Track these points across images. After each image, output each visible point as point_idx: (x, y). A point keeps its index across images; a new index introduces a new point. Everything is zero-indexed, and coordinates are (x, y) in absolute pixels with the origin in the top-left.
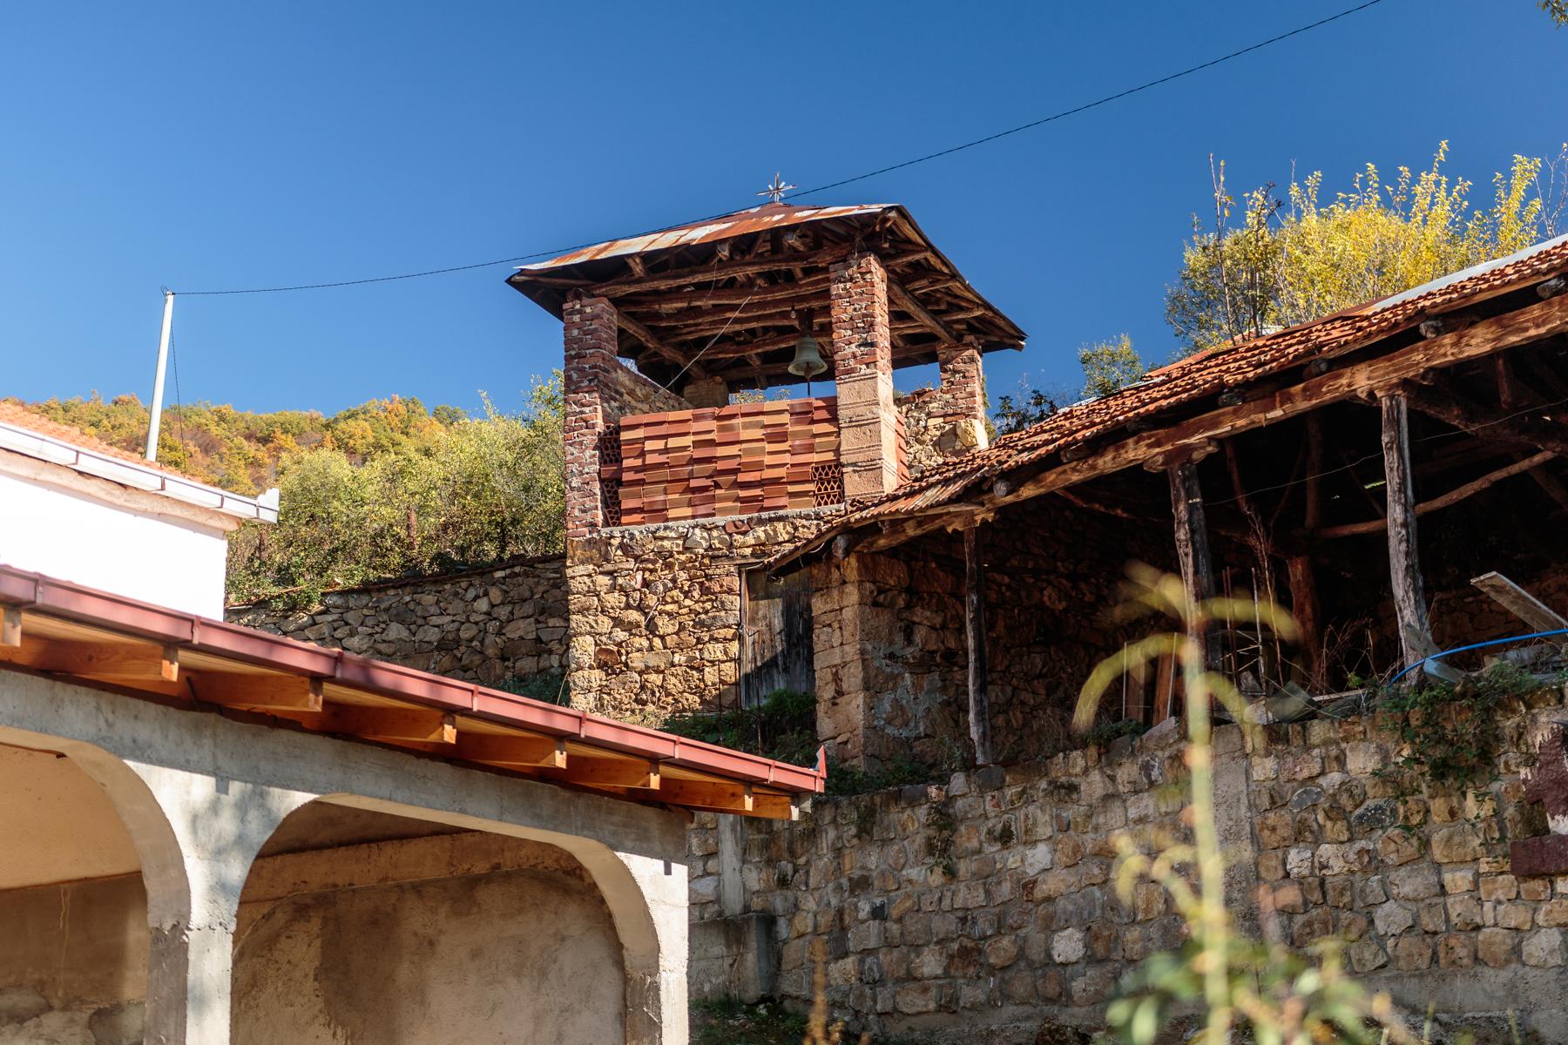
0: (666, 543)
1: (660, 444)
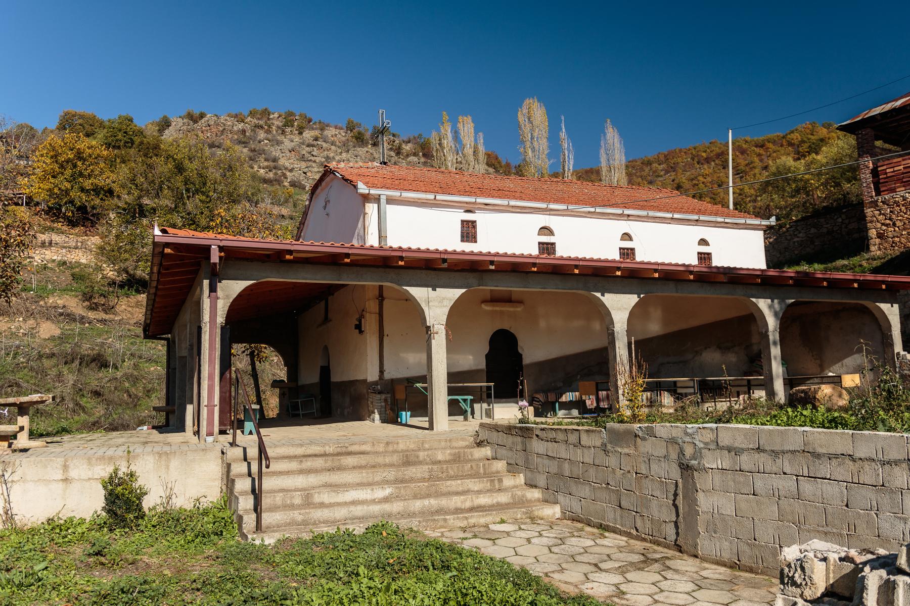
0: (897, 199)
1: (892, 170)
